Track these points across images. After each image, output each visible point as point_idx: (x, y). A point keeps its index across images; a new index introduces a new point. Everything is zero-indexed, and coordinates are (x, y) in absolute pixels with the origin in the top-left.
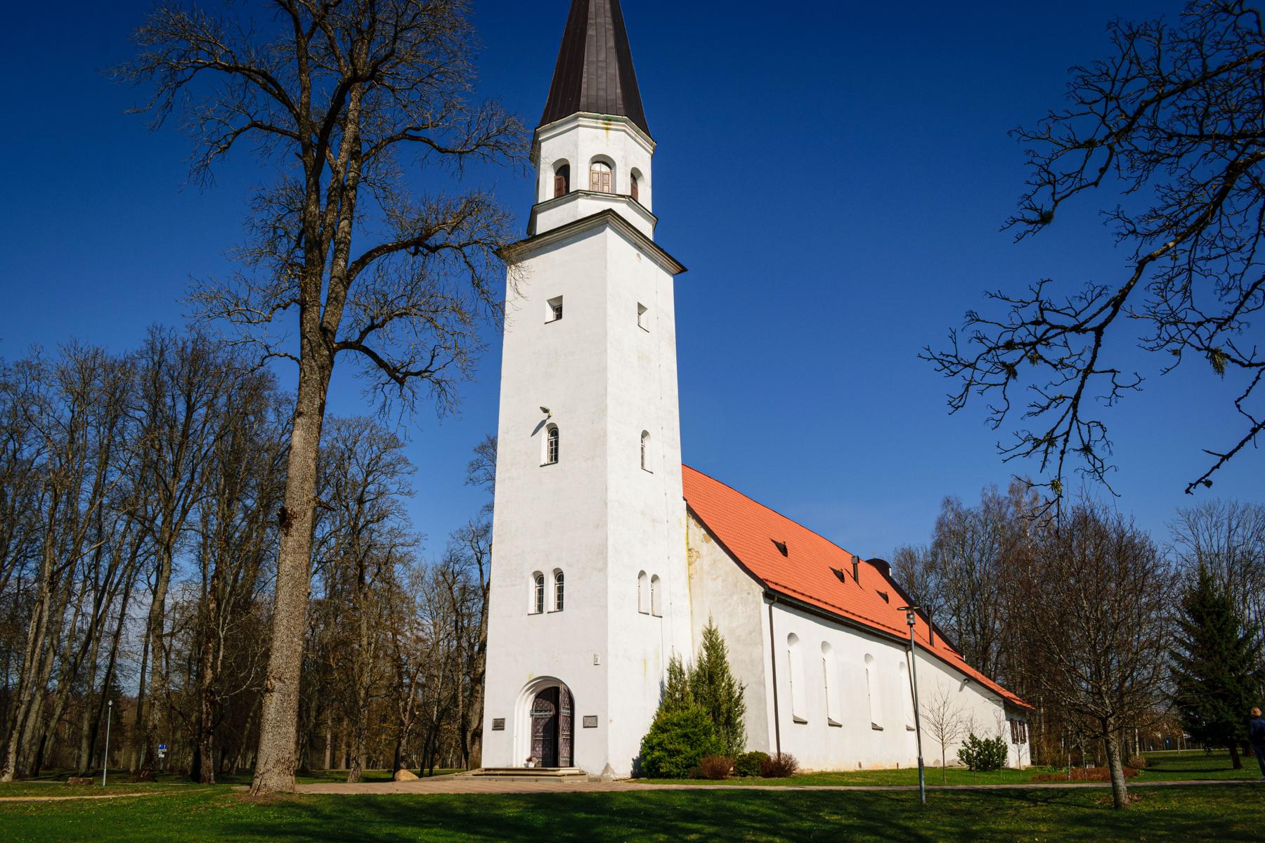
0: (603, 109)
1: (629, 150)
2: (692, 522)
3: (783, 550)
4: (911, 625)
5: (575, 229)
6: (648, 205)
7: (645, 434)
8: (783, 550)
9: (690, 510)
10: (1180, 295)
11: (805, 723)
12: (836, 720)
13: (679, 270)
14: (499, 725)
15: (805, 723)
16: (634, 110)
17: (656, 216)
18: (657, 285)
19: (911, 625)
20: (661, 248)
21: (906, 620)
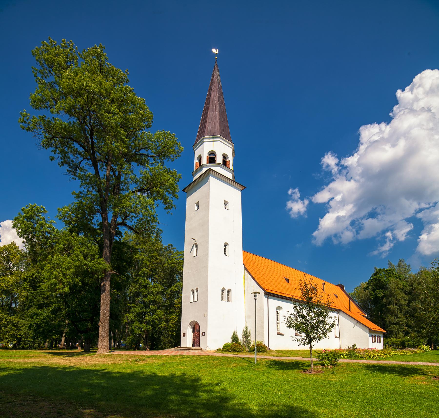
0: (213, 135)
1: (222, 148)
2: (246, 272)
3: (288, 281)
4: (256, 299)
5: (222, 178)
6: (231, 167)
7: (226, 245)
8: (288, 281)
9: (245, 267)
10: (101, 177)
11: (283, 335)
12: (281, 332)
13: (244, 190)
14: (184, 335)
15: (283, 335)
16: (225, 134)
17: (234, 172)
18: (235, 196)
19: (256, 299)
20: (236, 181)
21: (254, 298)
